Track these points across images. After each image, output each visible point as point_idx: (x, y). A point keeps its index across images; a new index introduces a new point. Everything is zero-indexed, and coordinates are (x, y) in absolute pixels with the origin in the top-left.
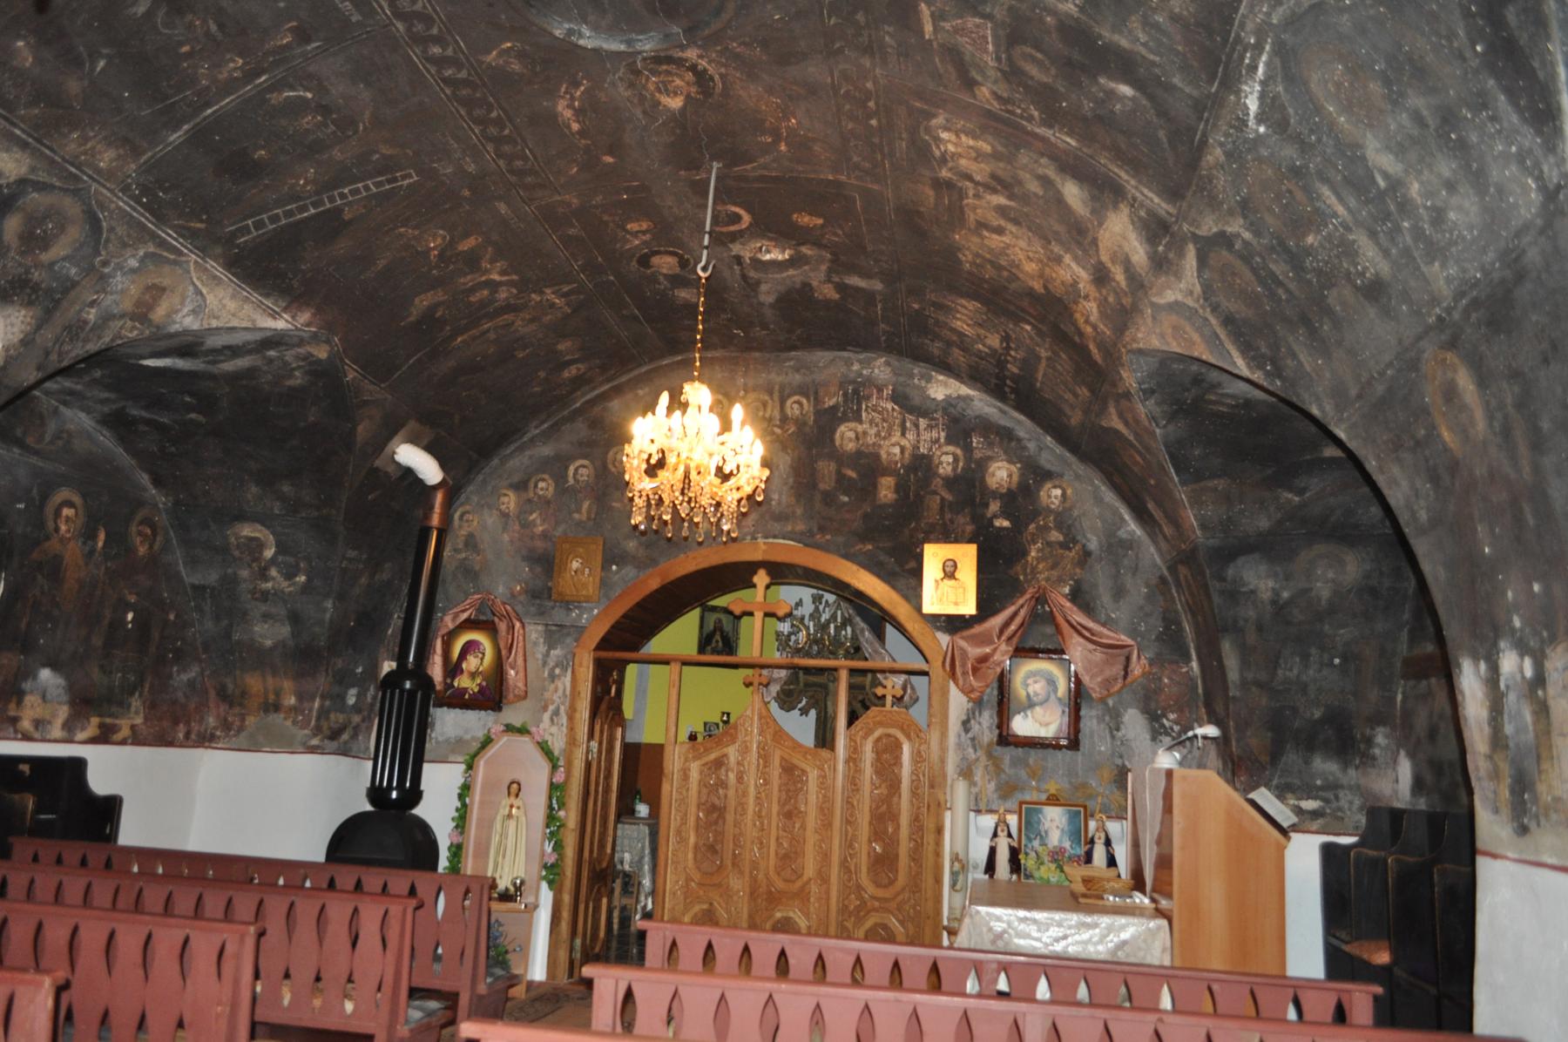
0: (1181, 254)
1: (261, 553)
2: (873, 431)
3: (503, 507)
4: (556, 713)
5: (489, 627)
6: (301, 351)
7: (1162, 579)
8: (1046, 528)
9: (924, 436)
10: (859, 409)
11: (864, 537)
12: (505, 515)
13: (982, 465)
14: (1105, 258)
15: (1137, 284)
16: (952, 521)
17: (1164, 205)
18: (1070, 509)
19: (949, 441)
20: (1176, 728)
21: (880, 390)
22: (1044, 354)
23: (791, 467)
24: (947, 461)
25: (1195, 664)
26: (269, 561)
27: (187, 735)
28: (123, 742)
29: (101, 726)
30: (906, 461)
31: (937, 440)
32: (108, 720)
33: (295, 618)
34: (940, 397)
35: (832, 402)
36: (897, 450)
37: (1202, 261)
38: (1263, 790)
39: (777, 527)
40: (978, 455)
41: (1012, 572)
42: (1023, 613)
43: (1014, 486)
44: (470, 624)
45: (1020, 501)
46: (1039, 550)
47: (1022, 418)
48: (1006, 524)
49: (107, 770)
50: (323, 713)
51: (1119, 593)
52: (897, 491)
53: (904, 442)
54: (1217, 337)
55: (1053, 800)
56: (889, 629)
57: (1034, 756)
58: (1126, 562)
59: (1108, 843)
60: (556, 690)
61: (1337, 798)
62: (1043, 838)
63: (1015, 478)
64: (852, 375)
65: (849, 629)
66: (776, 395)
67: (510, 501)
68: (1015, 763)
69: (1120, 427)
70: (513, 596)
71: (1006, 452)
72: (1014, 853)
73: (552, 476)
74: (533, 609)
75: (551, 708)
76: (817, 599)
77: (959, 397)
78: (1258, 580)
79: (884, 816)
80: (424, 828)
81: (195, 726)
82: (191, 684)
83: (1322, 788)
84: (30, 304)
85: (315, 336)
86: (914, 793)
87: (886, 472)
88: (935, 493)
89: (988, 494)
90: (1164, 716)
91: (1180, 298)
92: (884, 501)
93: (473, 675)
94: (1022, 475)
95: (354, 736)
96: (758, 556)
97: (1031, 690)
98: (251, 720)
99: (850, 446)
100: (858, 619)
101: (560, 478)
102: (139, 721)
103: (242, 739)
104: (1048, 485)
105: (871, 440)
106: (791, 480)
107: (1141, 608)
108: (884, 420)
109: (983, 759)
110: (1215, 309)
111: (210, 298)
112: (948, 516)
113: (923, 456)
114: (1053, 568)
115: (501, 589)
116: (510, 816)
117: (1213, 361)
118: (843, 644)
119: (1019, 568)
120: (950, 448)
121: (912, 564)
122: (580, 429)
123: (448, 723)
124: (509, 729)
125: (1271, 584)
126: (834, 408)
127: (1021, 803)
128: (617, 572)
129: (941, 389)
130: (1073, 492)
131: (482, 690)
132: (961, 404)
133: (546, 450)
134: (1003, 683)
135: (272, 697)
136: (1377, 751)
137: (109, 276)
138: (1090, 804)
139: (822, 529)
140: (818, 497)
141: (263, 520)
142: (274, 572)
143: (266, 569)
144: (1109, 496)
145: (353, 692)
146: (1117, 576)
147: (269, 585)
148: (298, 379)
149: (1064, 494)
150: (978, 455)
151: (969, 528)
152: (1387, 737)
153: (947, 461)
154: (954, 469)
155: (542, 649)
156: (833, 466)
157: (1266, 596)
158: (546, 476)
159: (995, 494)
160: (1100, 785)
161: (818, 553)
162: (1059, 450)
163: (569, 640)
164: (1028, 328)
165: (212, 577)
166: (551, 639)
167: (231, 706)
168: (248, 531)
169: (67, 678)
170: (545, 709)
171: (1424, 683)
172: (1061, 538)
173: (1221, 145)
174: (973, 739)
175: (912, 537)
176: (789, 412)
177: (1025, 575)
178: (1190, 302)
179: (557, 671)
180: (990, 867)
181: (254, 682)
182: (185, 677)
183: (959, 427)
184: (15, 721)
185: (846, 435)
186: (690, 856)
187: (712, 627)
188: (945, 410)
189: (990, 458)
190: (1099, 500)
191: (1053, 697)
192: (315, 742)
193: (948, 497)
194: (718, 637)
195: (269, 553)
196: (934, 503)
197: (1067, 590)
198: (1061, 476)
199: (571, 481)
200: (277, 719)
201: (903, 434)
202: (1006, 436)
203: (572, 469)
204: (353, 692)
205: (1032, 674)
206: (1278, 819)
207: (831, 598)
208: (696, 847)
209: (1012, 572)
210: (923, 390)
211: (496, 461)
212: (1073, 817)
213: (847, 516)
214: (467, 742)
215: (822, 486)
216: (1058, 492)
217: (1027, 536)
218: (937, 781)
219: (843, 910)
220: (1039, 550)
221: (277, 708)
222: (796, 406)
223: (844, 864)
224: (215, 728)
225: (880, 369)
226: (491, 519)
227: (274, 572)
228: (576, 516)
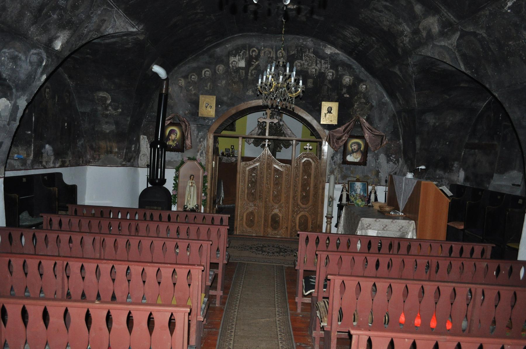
0: (454, 33)
1: (106, 101)
2: (306, 64)
3: (180, 84)
4: (202, 153)
5: (178, 125)
6: (135, 37)
7: (394, 115)
8: (360, 98)
9: (324, 66)
10: (302, 56)
12: (181, 87)
13: (341, 76)
14: (420, 27)
15: (430, 37)
16: (331, 95)
17: (455, 19)
19: (331, 68)
20: (394, 160)
21: (309, 50)
22: (376, 46)
24: (330, 75)
25: (401, 141)
26: (107, 103)
28: (67, 166)
29: (62, 161)
32: (63, 159)
33: (117, 123)
34: (329, 53)
35: (293, 53)
36: (314, 70)
37: (461, 37)
38: (444, 187)
40: (340, 73)
42: (351, 125)
43: (351, 84)
44: (171, 124)
45: (353, 88)
46: (357, 105)
47: (355, 61)
48: (348, 96)
49: (69, 176)
50: (126, 154)
51: (381, 119)
52: (313, 84)
54: (457, 59)
55: (358, 180)
57: (352, 167)
59: (375, 193)
60: (201, 146)
61: (442, 181)
62: (355, 191)
63: (351, 81)
66: (274, 50)
67: (182, 82)
68: (346, 169)
69: (398, 72)
70: (185, 114)
72: (348, 195)
73: (196, 74)
74: (192, 119)
75: (200, 151)
77: (335, 53)
78: (431, 120)
79: (305, 185)
80: (167, 191)
81: (84, 159)
82: (82, 145)
83: (438, 178)
84: (69, 29)
85: (142, 33)
86: (315, 177)
87: (310, 77)
88: (326, 85)
89: (342, 86)
90: (391, 156)
91: (446, 45)
93: (173, 141)
94: (353, 81)
95: (134, 160)
98: (102, 156)
101: (199, 75)
102: (71, 159)
105: (305, 66)
108: (310, 60)
109: (337, 168)
110: (459, 51)
111: (118, 23)
112: (330, 93)
114: (362, 110)
115: (181, 112)
116: (192, 186)
117: (451, 64)
120: (331, 71)
121: (318, 108)
122: (205, 58)
123: (170, 156)
124: (190, 159)
125: (434, 121)
126: (294, 55)
127: (349, 181)
128: (220, 108)
129: (329, 50)
130: (372, 88)
131: (177, 145)
133: (194, 65)
134: (345, 145)
135: (109, 149)
136: (454, 168)
137: (93, 17)
138: (369, 181)
141: (107, 91)
142: (110, 108)
143: (108, 107)
144: (380, 88)
145: (133, 146)
147: (108, 112)
148: (130, 45)
149: (366, 87)
150: (340, 73)
151: (336, 97)
152: (457, 164)
153: (330, 75)
154: (332, 77)
155: (196, 132)
157: (431, 124)
158: (194, 74)
159: (345, 86)
160: (372, 176)
162: (366, 73)
163: (205, 130)
164: (374, 38)
165: (88, 110)
167: (95, 151)
168: (101, 94)
169: (52, 147)
170: (198, 152)
171: (473, 151)
173: (490, 10)
174: (334, 162)
178: (450, 47)
179: (202, 140)
180: (341, 199)
181: (103, 144)
182: (80, 143)
183: (335, 64)
184: (41, 162)
186: (246, 196)
189: (344, 75)
192: (124, 163)
193: (330, 87)
195: (109, 102)
197: (365, 118)
198: (366, 81)
199: (203, 76)
200: (111, 156)
201: (316, 65)
203: (203, 71)
204: (133, 146)
206: (447, 194)
208: (248, 193)
210: (324, 51)
211: (176, 68)
212: (364, 185)
214: (172, 162)
216: (365, 86)
218: (323, 174)
219: (293, 211)
220: (357, 105)
221: (111, 152)
223: (294, 197)
224: (90, 159)
225: (309, 42)
226: (176, 89)
227: (110, 108)
228: (206, 88)
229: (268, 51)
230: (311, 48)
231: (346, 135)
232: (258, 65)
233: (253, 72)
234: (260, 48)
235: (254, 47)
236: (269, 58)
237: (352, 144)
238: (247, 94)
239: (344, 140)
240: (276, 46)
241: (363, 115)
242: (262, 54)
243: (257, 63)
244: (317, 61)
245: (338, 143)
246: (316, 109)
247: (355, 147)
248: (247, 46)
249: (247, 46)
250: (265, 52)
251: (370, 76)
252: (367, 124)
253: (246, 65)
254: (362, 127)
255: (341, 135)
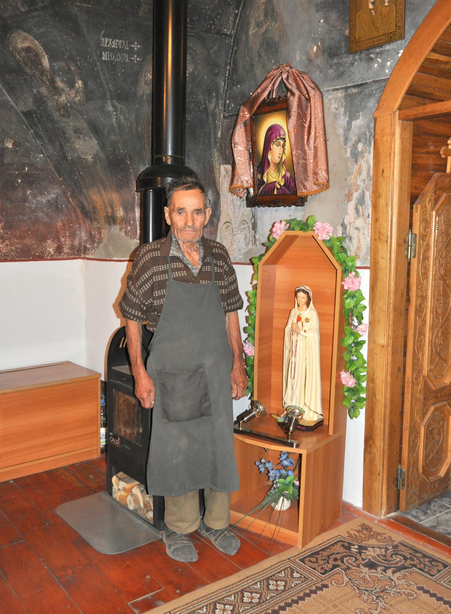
4: (361, 201)
27: (59, 249)
70: (310, 61)
75: (356, 195)
93: (278, 166)
103: (99, 252)
155: (343, 121)
166: (352, 108)
170: (349, 197)
179: (360, 147)
224: (86, 241)
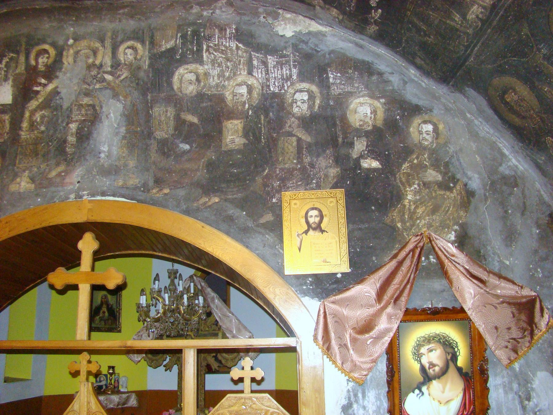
2: (215, 72)
8: (421, 167)
10: (200, 50)
11: (209, 189)
13: (341, 102)
16: (312, 165)
18: (446, 144)
21: (222, 29)
23: (123, 115)
24: (301, 99)
30: (255, 102)
31: (289, 78)
34: (289, 33)
36: (243, 90)
39: (105, 182)
40: (335, 91)
41: (387, 220)
42: (404, 268)
43: (380, 123)
45: (388, 138)
46: (415, 193)
47: (382, 50)
48: (375, 164)
51: (510, 236)
52: (246, 134)
53: (251, 81)
56: (234, 293)
58: (512, 200)
63: (381, 115)
64: (191, 18)
65: (201, 298)
71: (367, 87)
76: (173, 275)
77: (310, 33)
88: (290, 134)
89: (349, 133)
92: (232, 146)
94: (387, 110)
96: (80, 217)
97: (425, 361)
99: (191, 89)
100: (209, 290)
104: (417, 121)
105: (213, 81)
106: (123, 130)
107: (536, 252)
108: (228, 60)
112: (307, 160)
113: (274, 93)
118: (197, 312)
119: (395, 214)
120: (305, 85)
121: (269, 217)
126: (172, 51)
132: (313, 41)
134: (393, 353)
139: (158, 182)
140: (154, 146)
146: (505, 217)
150: (335, 91)
151: (334, 172)
153: (301, 99)
154: (311, 107)
156: (171, 112)
159: (359, 133)
161: (154, 209)
162: (426, 82)
172: (440, 178)
175: (265, 185)
176: (121, 58)
177: (403, 221)
183: (313, 65)
185: (185, 79)
187: (99, 302)
188: (295, 47)
189: (350, 94)
190: (474, 135)
191: (451, 365)
193: (307, 138)
194: (104, 309)
196: (289, 146)
197: (452, 236)
201: (250, 73)
202: (366, 69)
205: (429, 340)
207: (186, 272)
209: (387, 220)
210: (271, 27)
213: (188, 166)
215: (160, 134)
216: (430, 127)
217: (401, 176)
222: (129, 51)
229: (89, 47)
230: (228, 25)
231: (389, 309)
232: (56, 92)
233: (38, 117)
234: (61, 43)
235: (44, 42)
236: (89, 67)
237: (419, 346)
238: (13, 188)
239: (387, 331)
240: (115, 34)
241: (443, 227)
242: (68, 59)
243: (50, 87)
244: (250, 60)
245: (361, 352)
246: (262, 221)
247: (434, 357)
248: (23, 40)
249: (23, 40)
250: (77, 53)
251: (441, 90)
252: (461, 258)
253: (15, 98)
254: (445, 274)
255: (372, 311)
